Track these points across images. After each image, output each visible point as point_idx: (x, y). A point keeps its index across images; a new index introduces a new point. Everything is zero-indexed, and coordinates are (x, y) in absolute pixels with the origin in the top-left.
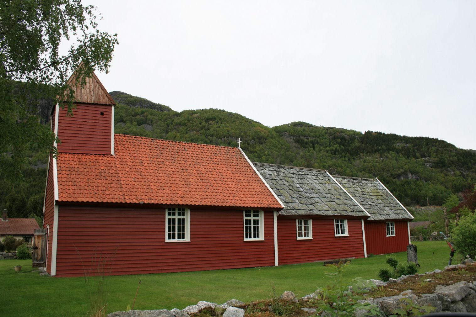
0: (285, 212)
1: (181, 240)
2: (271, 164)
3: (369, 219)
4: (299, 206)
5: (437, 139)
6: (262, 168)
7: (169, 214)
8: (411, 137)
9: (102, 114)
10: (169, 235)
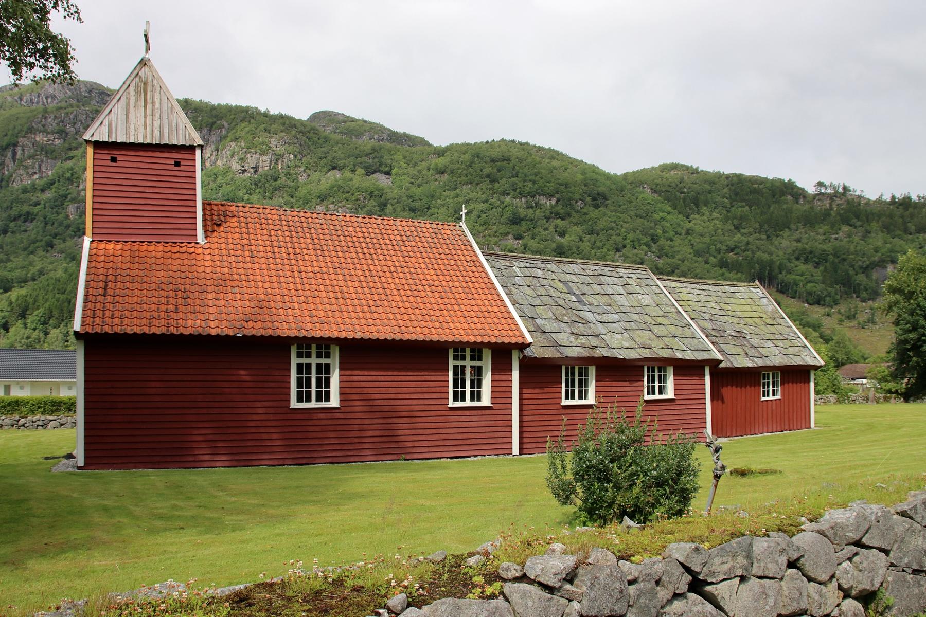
1: (323, 405)
7: (299, 355)
9: (177, 164)
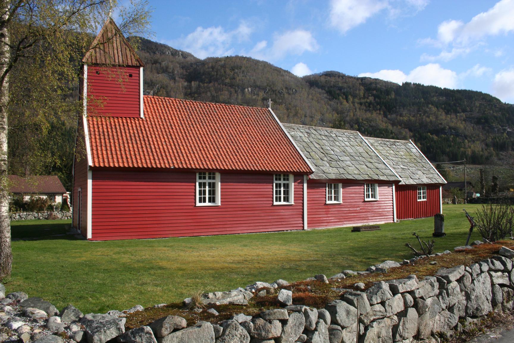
0: (315, 176)
2: (301, 126)
3: (400, 184)
4: (330, 170)
5: (481, 93)
6: (293, 130)
8: (452, 89)
10: (200, 199)
